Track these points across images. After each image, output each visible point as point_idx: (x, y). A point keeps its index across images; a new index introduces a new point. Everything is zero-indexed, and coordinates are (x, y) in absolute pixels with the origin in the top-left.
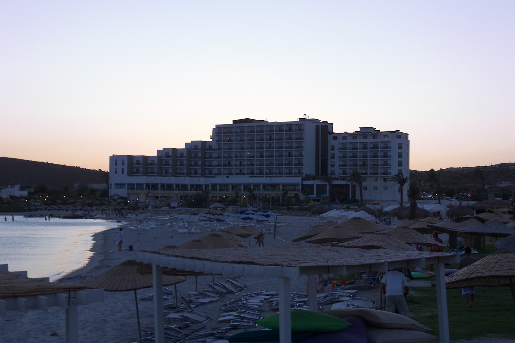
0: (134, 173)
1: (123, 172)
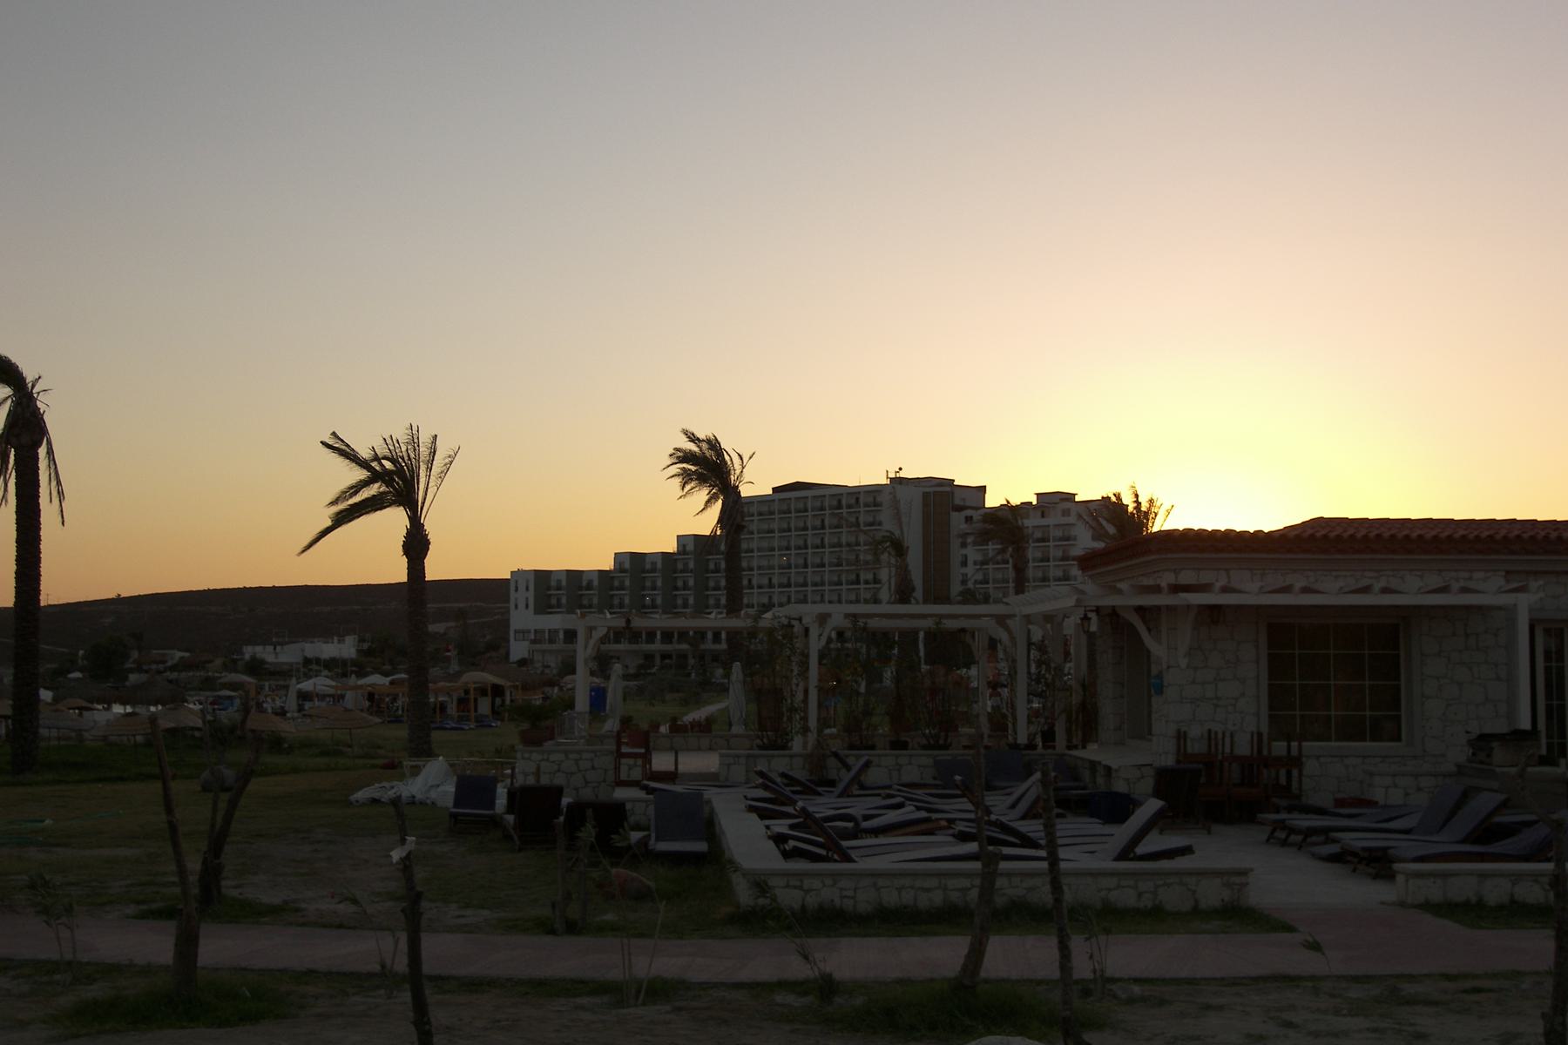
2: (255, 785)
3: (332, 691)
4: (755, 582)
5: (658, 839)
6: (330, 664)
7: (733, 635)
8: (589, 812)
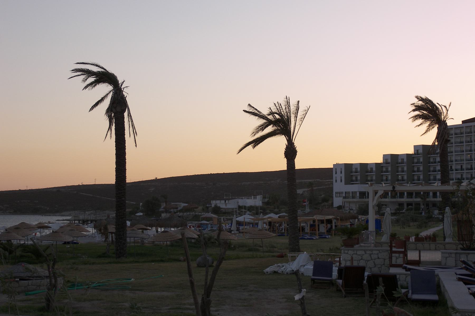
0: (354, 181)
1: (341, 181)
2: (224, 264)
3: (252, 221)
4: (454, 168)
5: (412, 293)
6: (251, 209)
7: (445, 194)
8: (381, 279)
